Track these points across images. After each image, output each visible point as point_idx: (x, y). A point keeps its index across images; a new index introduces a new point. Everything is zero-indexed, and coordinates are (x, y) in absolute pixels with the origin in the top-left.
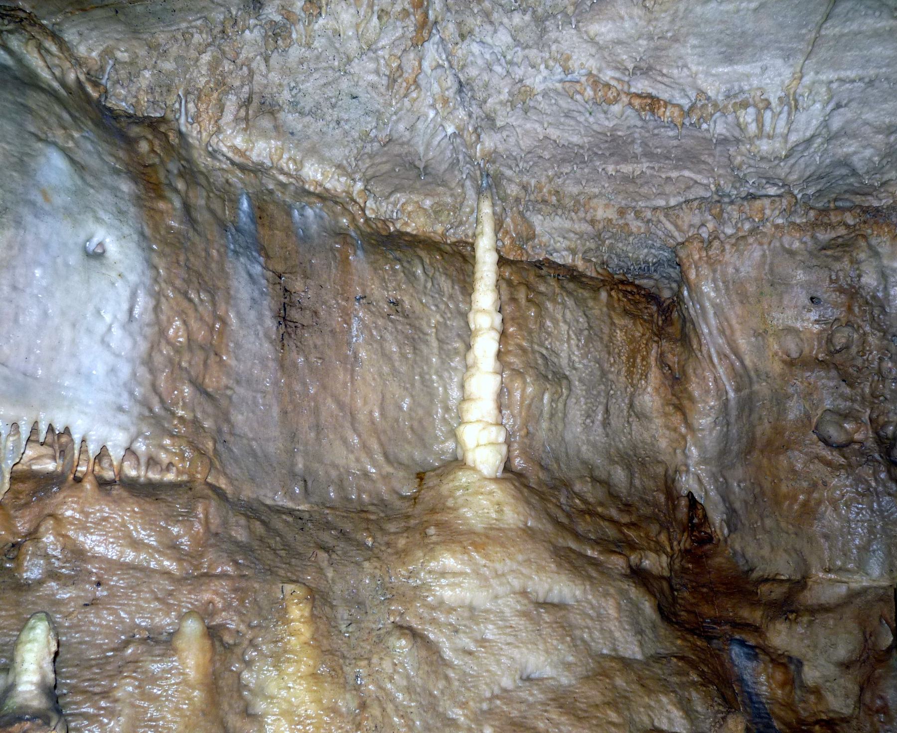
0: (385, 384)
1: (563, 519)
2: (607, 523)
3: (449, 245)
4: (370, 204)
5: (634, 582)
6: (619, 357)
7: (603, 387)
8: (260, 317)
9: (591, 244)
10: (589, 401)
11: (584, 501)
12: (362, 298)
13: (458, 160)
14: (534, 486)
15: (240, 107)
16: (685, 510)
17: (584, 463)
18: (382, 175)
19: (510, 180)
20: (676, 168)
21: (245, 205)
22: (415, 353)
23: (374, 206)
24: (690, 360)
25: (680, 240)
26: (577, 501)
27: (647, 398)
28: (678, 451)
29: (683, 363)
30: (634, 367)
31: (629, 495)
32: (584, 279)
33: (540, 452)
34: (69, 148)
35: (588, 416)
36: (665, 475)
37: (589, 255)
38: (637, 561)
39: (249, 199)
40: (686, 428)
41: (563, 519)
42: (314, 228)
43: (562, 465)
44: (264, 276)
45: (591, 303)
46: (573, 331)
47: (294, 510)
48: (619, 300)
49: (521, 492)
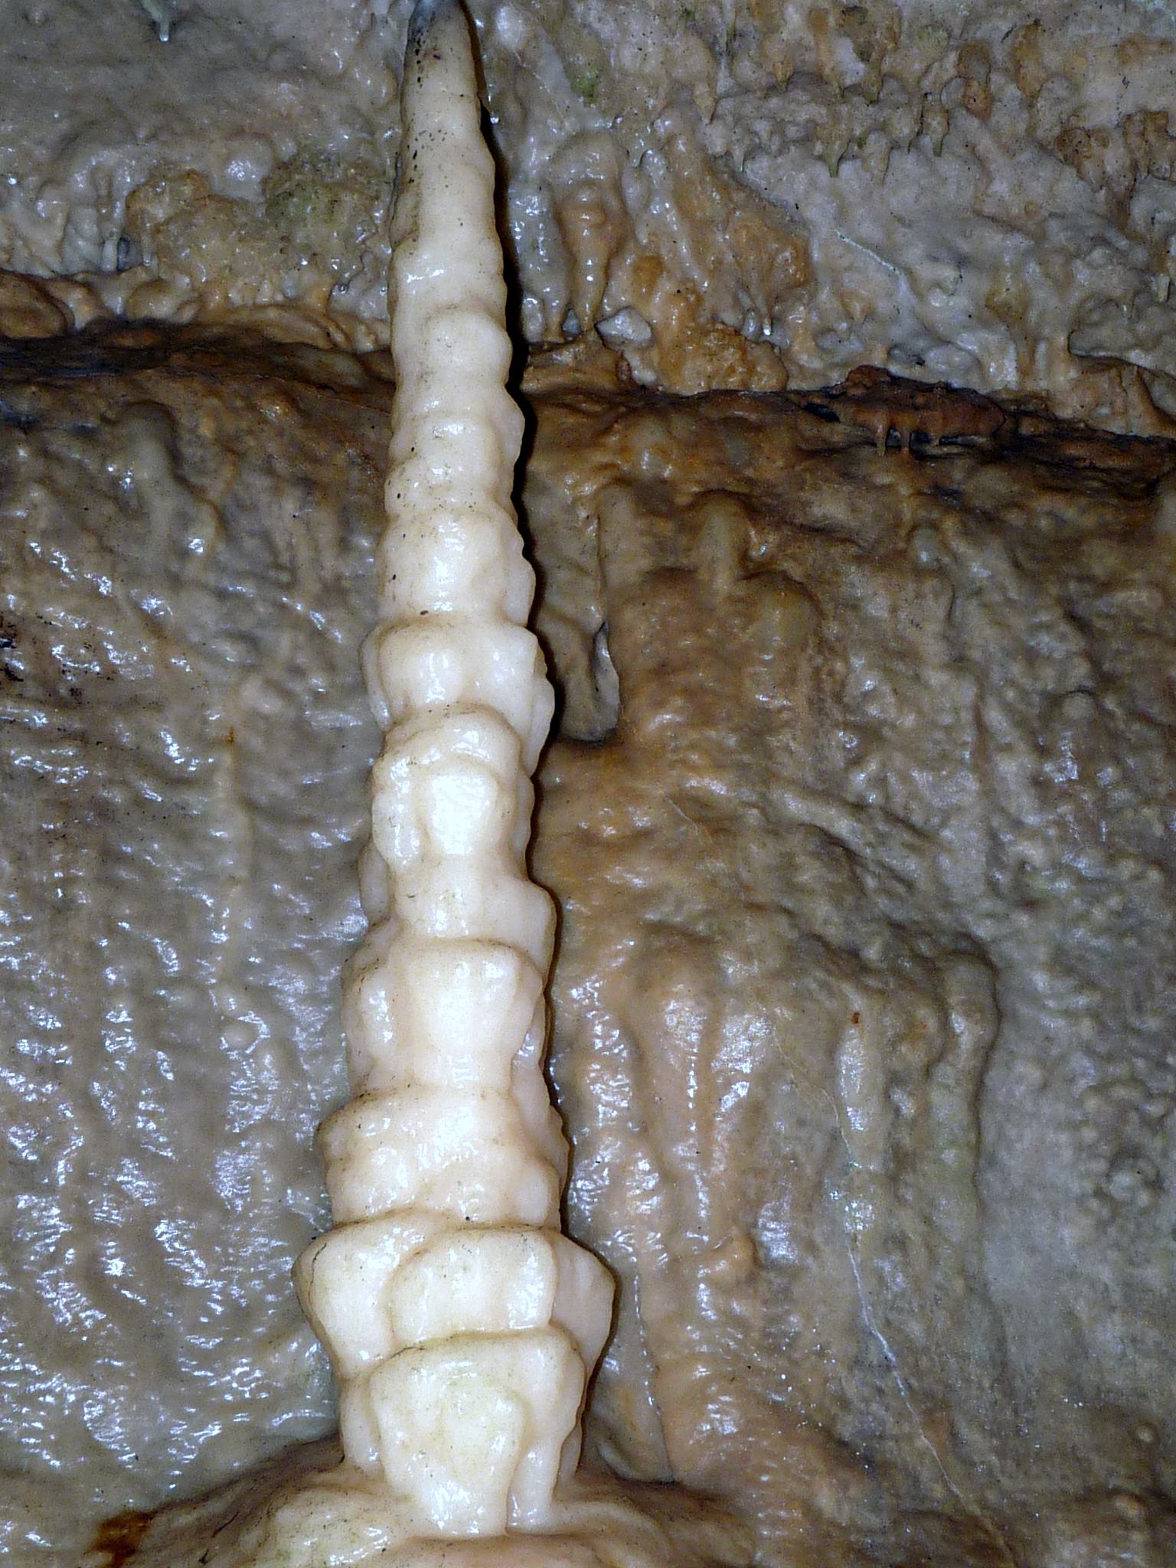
10: (1120, 1070)
22: (105, 881)
32: (1073, 450)
33: (833, 1365)
35: (1125, 1155)
37: (1109, 336)
43: (969, 1434)
45: (1103, 559)
46: (1008, 708)
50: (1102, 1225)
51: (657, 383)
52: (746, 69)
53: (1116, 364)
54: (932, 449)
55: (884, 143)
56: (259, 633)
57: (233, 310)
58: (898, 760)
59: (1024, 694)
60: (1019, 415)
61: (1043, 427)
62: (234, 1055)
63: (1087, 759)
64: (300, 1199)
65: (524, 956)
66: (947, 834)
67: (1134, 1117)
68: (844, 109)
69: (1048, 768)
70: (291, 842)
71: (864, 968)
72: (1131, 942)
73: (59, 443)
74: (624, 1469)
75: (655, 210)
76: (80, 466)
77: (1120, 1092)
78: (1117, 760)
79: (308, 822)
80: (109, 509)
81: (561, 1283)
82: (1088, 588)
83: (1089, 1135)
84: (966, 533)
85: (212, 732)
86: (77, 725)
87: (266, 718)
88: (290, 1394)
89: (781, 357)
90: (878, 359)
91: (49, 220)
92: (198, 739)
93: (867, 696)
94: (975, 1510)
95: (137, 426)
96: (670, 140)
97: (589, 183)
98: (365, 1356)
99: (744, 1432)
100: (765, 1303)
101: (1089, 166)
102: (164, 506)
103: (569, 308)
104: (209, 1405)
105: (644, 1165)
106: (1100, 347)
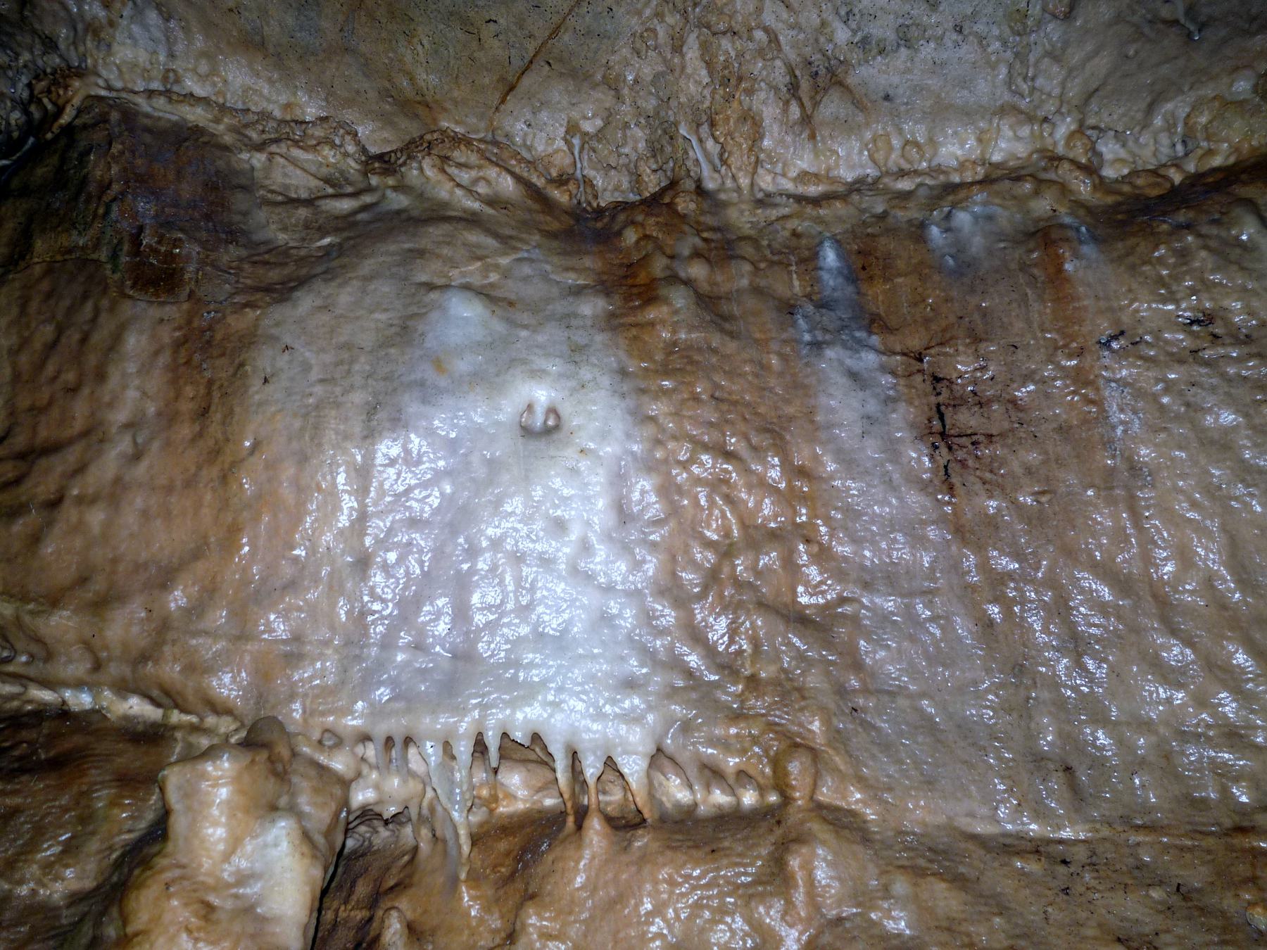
0: (1228, 510)
4: (1109, 149)
8: (892, 450)
12: (1114, 338)
15: (787, 103)
18: (1104, 84)
21: (830, 257)
23: (1123, 154)
34: (492, 285)
39: (838, 243)
42: (977, 244)
44: (883, 369)
47: (1050, 842)
73: (1205, 229)
76: (1218, 237)
80: (1238, 251)
95: (1238, 211)
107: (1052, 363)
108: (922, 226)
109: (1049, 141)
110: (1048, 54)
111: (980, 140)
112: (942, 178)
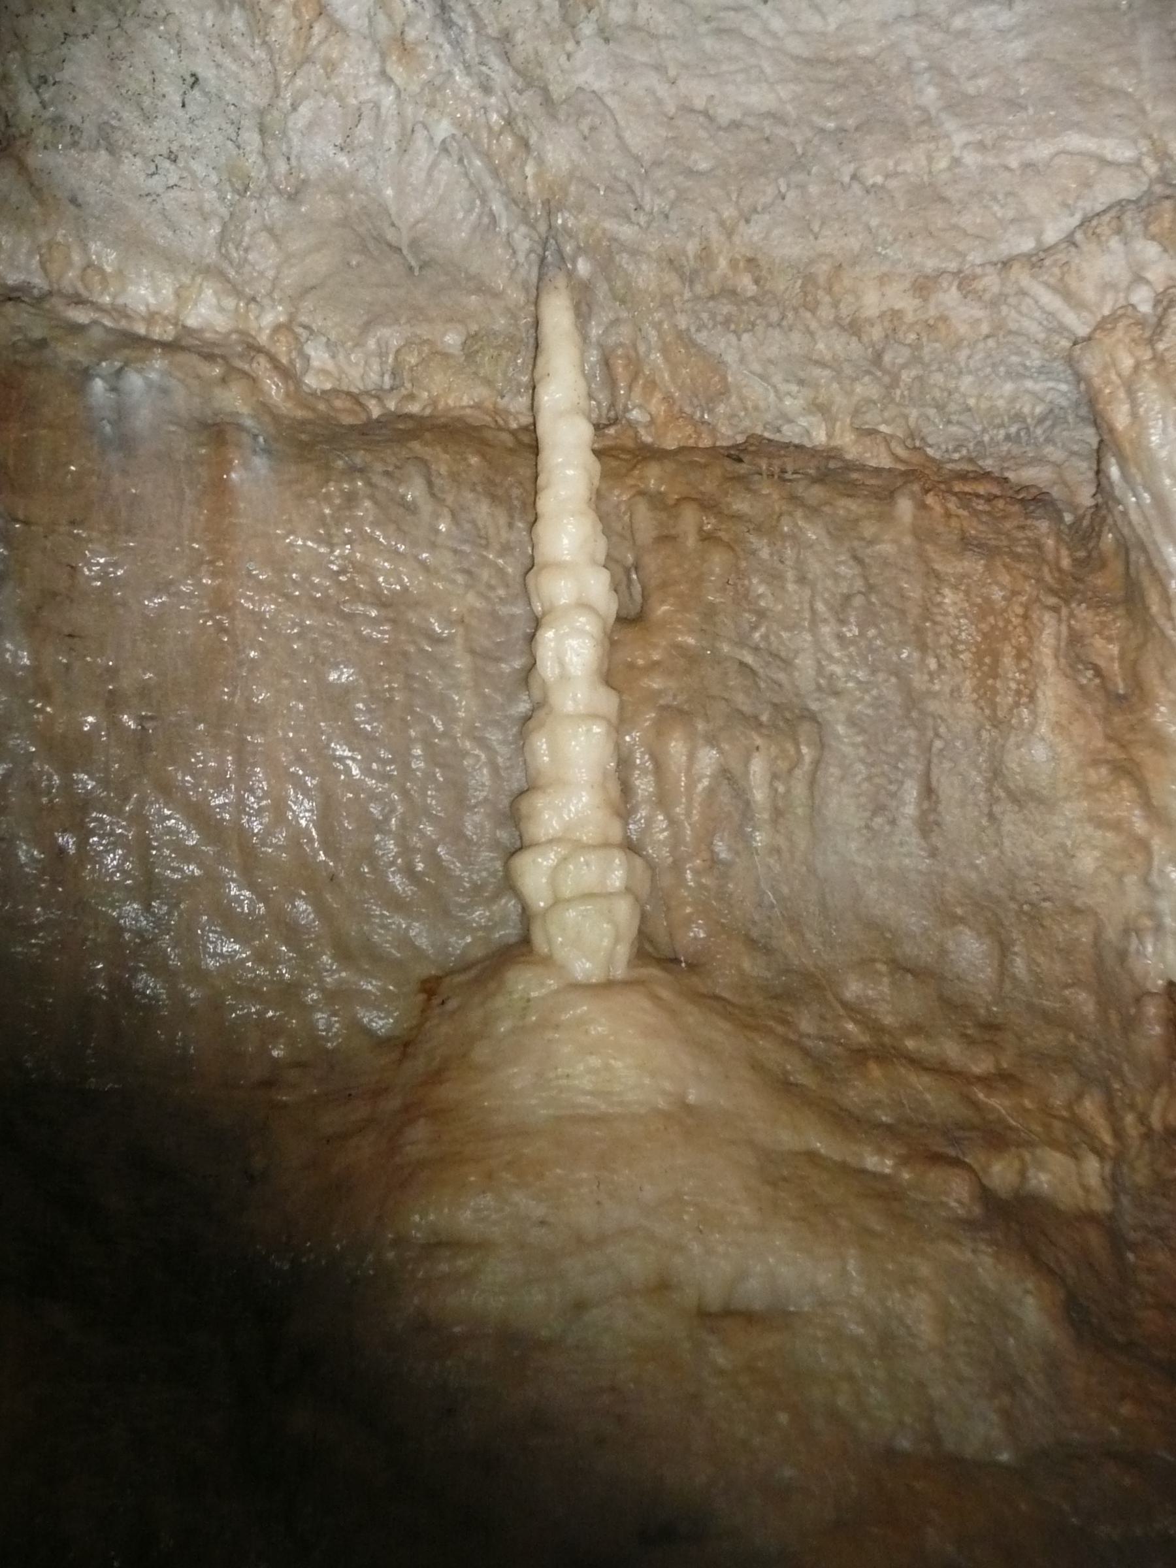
1: (806, 1078)
2: (926, 1079)
3: (513, 433)
4: (318, 355)
5: (992, 1242)
6: (955, 654)
7: (911, 733)
9: (866, 389)
11: (874, 1027)
13: (493, 217)
14: (726, 994)
16: (1158, 1030)
17: (871, 924)
19: (635, 252)
20: (1041, 131)
24: (1150, 646)
25: (1082, 331)
26: (850, 1026)
27: (1040, 752)
28: (1131, 880)
29: (1132, 656)
30: (995, 676)
31: (1000, 999)
32: (854, 476)
36: (1096, 944)
37: (871, 418)
38: (1011, 1178)
40: (1147, 818)
41: (806, 1078)
42: (143, 418)
43: (809, 936)
45: (869, 529)
46: (826, 602)
48: (948, 515)
49: (673, 1013)
50: (868, 841)
51: (653, 444)
52: (699, 288)
53: (872, 432)
54: (788, 476)
55: (764, 324)
56: (473, 569)
57: (451, 409)
58: (775, 627)
59: (833, 595)
60: (829, 458)
61: (840, 464)
62: (470, 770)
63: (862, 626)
64: (503, 835)
65: (609, 722)
66: (797, 661)
67: (883, 792)
68: (745, 308)
69: (844, 629)
70: (491, 669)
71: (761, 725)
72: (882, 711)
73: (376, 479)
74: (655, 954)
75: (652, 357)
76: (387, 491)
77: (877, 780)
78: (876, 626)
79: (498, 660)
80: (401, 511)
81: (630, 872)
82: (863, 543)
83: (863, 800)
84: (806, 518)
85: (454, 618)
86: (392, 615)
87: (478, 610)
88: (504, 921)
89: (713, 430)
90: (759, 430)
91: (357, 364)
92: (448, 622)
93: (760, 596)
94: (812, 969)
95: (412, 469)
96: (661, 323)
97: (621, 345)
98: (542, 904)
99: (709, 936)
100: (717, 878)
101: (865, 339)
102: (426, 508)
103: (612, 405)
104: (464, 927)
105: (661, 817)
106: (866, 423)
107: (193, 576)
108: (86, 374)
109: (253, 324)
110: (270, 230)
111: (177, 295)
112: (123, 323)
